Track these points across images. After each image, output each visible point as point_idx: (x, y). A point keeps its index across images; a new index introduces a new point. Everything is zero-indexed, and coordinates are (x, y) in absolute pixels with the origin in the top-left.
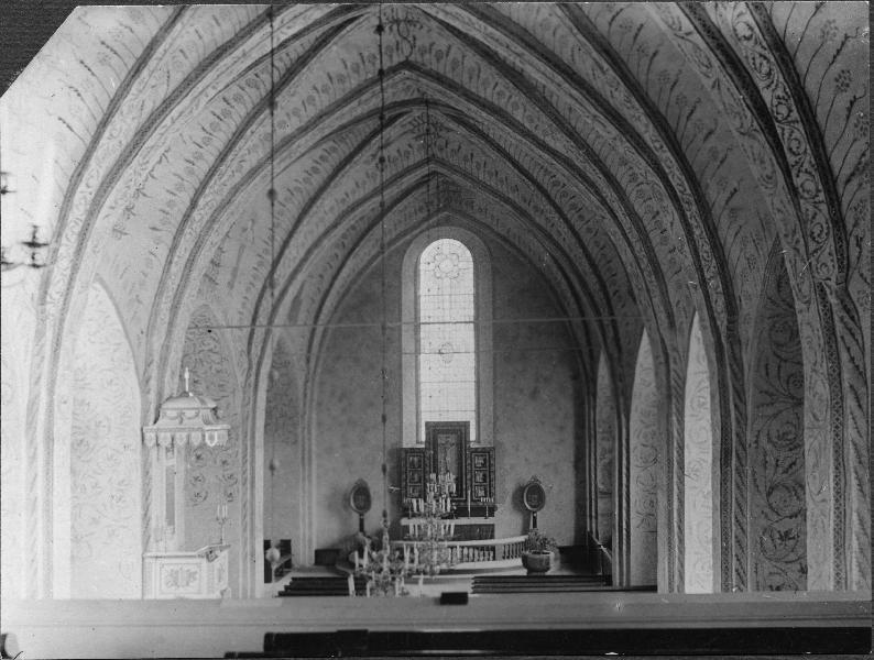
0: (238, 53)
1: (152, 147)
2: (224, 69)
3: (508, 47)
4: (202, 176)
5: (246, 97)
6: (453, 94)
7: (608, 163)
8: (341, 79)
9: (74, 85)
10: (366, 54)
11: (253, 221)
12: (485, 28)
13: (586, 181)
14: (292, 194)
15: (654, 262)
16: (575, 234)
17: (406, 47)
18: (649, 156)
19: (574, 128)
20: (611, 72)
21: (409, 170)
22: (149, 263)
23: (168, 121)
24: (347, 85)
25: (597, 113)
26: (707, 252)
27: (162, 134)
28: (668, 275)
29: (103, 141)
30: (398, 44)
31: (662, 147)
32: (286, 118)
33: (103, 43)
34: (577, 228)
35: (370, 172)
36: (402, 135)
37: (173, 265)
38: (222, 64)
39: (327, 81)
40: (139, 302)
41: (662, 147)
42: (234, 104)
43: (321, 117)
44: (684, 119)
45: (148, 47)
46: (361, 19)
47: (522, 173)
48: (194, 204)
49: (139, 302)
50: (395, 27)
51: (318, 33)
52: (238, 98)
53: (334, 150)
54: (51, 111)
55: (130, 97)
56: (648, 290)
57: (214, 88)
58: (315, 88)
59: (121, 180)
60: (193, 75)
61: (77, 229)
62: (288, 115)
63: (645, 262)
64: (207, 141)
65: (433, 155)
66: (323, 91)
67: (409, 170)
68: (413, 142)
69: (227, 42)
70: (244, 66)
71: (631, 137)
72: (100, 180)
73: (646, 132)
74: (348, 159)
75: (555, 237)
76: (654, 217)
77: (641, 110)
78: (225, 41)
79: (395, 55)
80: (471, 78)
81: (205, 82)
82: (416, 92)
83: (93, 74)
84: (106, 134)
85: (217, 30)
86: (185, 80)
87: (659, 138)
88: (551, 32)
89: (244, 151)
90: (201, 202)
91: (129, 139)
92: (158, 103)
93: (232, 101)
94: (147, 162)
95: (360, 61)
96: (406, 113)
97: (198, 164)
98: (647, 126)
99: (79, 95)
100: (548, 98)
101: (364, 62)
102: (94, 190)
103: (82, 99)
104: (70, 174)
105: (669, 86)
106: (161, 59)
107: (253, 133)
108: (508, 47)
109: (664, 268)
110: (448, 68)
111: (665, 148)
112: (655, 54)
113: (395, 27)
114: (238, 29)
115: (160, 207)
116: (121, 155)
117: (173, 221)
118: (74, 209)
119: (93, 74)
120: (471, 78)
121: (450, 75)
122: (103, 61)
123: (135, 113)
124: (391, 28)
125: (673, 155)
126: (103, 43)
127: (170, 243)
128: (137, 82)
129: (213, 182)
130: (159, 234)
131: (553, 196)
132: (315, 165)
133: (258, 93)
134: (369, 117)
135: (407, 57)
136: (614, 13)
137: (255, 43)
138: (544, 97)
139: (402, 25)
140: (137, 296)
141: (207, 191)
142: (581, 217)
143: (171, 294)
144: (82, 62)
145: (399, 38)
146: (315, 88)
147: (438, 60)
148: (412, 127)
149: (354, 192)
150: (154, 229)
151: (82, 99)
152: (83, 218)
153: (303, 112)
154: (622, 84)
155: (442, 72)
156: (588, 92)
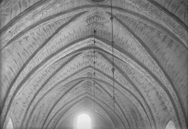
0: (57, 56)
1: (31, 78)
2: (52, 60)
3: (126, 58)
4: (37, 90)
5: (51, 71)
6: (101, 74)
7: (141, 91)
8: (74, 69)
9: (15, 59)
10: (80, 63)
11: (43, 105)
12: (121, 54)
13: (134, 96)
14: (53, 99)
15: (152, 117)
16: (123, 112)
17: (90, 62)
18: (163, 86)
19: (133, 83)
20: (156, 64)
21: (81, 95)
22: (21, 112)
23: (37, 72)
24: (75, 70)
25: (149, 75)
26: (180, 111)
27: (34, 75)
28: (156, 120)
29: (20, 75)
30: (88, 61)
31: (168, 83)
32: (59, 78)
33: (24, 49)
34: (123, 110)
35: (72, 95)
36: (157, 51)
37: (28, 113)
38: (52, 58)
39: (70, 69)
40: (18, 122)
41: (168, 83)
42: (48, 72)
43: (67, 78)
44: (174, 76)
45: (36, 51)
46: (83, 53)
47: (110, 96)
48: (34, 97)
49: (18, 122)
50: (88, 57)
51: (69, 57)
52: (49, 71)
53: (65, 89)
54: (8, 66)
55: (29, 64)
56: (151, 124)
57: (49, 65)
58: (67, 70)
59: (22, 87)
60: (45, 60)
61: (10, 99)
62: (60, 77)
63: (150, 117)
64: (40, 81)
65: (87, 92)
66: (69, 71)
67: (81, 95)
68: (83, 88)
69: (54, 53)
70: (57, 60)
71: (158, 81)
72: (18, 85)
73: (164, 80)
74: (68, 91)
75: (117, 113)
76: (153, 106)
77: (164, 74)
78: (54, 53)
79: (87, 64)
80: (106, 70)
81: (47, 63)
82: (87, 76)
83: (20, 57)
84: (21, 73)
85: (52, 50)
86: (42, 62)
87: (168, 81)
88: (138, 54)
89: (49, 85)
90: (37, 97)
91: (26, 76)
92: (35, 66)
93: (47, 72)
94: (29, 82)
95: (79, 65)
96: (84, 80)
97: (37, 87)
98: (164, 78)
99: (16, 62)
100: (127, 75)
101: (79, 65)
102: (15, 88)
103: (16, 63)
104: (10, 83)
105: (171, 68)
106: (39, 54)
107: (52, 80)
108: (126, 58)
109: (155, 118)
110: (100, 67)
111: (169, 84)
112: (168, 60)
113: (88, 57)
114: (57, 50)
115: (26, 97)
116: (23, 80)
117: (29, 101)
118: (10, 93)
119: (20, 57)
120: (106, 70)
121: (100, 69)
122: (24, 54)
123: (29, 69)
124: (87, 57)
125: (171, 85)
126: (24, 49)
127: (27, 107)
128: (31, 60)
129: (40, 92)
130: (25, 104)
131: (118, 102)
132: (59, 92)
133: (54, 70)
134: (76, 80)
135: (90, 65)
136: (157, 50)
137: (61, 54)
138: (126, 75)
139: (90, 57)
140: (18, 121)
141: (38, 94)
142: (124, 108)
143: (26, 121)
144: (18, 54)
145: (89, 60)
146: (67, 70)
147: (98, 66)
148: (83, 85)
149: (67, 100)
150: (24, 103)
151: (16, 63)
152: (12, 95)
153: (63, 76)
154: (159, 67)
155: (99, 69)
156: (147, 70)
